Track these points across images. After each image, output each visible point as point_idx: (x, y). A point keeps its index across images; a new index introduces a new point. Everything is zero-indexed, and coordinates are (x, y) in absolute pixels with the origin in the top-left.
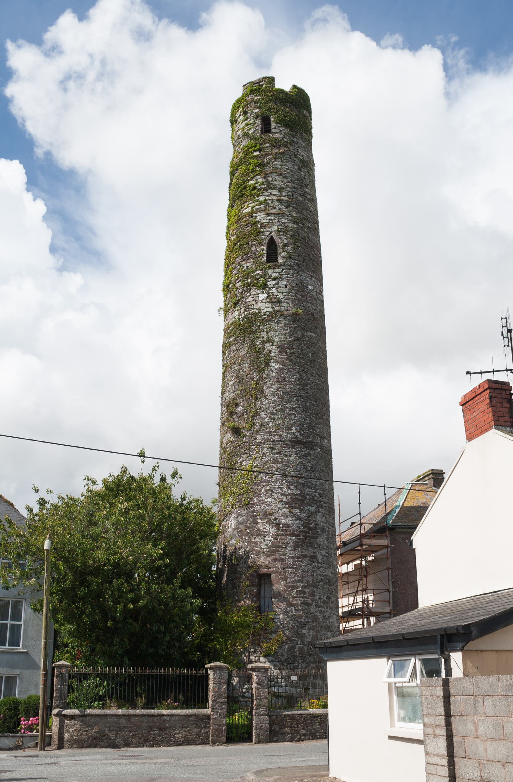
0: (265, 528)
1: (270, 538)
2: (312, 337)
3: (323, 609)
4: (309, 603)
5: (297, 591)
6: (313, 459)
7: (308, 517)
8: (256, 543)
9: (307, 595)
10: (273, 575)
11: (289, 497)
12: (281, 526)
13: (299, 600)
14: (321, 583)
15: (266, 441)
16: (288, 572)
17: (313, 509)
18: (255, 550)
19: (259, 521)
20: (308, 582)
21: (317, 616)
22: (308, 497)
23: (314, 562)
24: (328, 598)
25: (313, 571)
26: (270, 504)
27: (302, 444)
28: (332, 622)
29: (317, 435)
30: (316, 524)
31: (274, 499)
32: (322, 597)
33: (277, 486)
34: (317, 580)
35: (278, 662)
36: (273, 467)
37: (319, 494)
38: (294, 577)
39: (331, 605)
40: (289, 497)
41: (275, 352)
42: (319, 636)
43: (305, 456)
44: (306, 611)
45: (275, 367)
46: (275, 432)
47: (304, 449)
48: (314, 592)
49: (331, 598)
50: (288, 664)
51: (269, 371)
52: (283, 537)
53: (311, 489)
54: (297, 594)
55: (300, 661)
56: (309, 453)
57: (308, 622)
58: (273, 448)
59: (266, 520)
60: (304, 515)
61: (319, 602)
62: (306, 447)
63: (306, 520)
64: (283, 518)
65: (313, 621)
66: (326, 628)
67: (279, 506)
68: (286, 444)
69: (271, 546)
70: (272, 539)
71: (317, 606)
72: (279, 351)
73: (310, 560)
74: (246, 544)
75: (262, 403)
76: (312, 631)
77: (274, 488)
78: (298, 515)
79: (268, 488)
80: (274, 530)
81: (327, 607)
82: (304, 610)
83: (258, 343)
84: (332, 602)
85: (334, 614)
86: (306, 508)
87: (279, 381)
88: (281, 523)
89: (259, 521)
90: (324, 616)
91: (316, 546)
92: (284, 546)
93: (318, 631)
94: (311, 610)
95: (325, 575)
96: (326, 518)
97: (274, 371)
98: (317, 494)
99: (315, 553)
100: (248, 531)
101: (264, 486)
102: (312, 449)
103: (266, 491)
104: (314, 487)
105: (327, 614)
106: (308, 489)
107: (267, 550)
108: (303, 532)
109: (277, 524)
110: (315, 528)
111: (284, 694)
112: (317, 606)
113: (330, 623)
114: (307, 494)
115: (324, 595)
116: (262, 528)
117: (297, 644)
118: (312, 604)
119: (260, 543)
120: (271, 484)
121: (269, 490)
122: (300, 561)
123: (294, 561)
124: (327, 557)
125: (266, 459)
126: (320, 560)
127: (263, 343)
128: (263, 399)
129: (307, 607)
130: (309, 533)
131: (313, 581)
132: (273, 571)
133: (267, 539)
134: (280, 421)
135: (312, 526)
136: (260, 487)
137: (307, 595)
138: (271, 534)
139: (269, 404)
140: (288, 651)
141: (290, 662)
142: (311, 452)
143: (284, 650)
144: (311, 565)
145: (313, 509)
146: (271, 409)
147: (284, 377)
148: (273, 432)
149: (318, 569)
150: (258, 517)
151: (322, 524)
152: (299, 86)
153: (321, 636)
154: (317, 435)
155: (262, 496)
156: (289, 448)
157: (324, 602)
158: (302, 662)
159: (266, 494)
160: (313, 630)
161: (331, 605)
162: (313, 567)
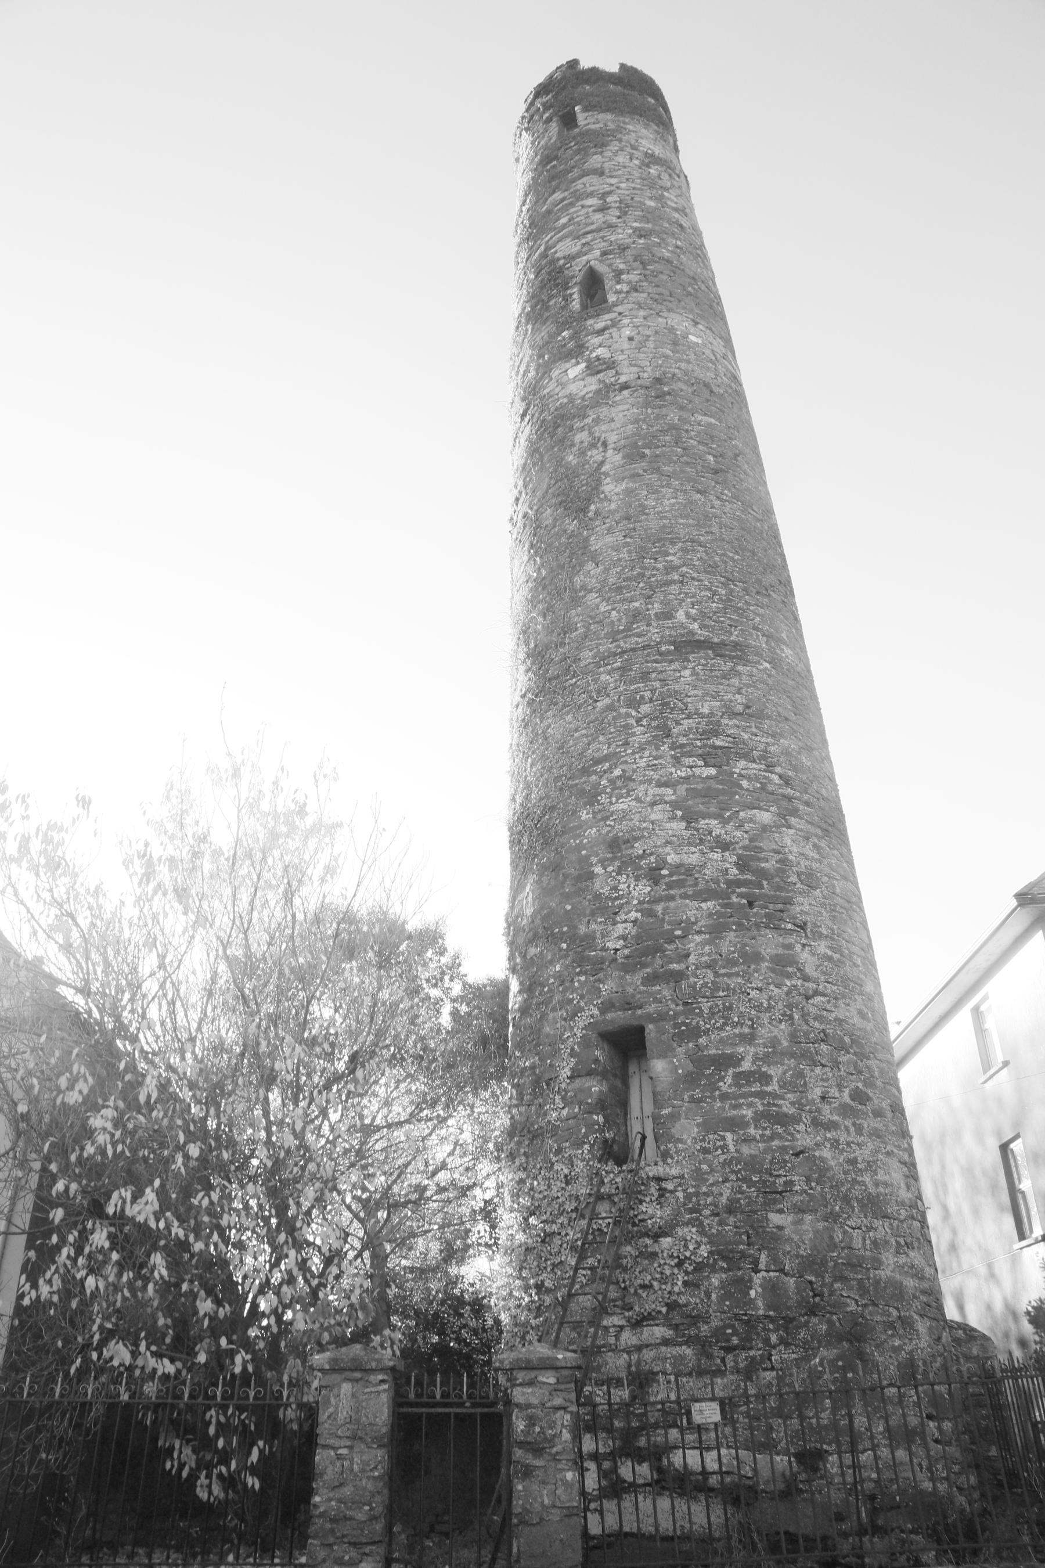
0: (615, 888)
1: (634, 915)
2: (710, 424)
3: (843, 1137)
4: (786, 1115)
5: (737, 1076)
6: (748, 686)
7: (751, 840)
8: (591, 937)
9: (774, 1087)
10: (650, 1027)
11: (682, 790)
12: (665, 872)
13: (750, 1105)
14: (824, 1047)
15: (603, 659)
16: (701, 1015)
17: (765, 817)
18: (589, 958)
19: (598, 870)
20: (774, 1042)
21: (822, 1159)
22: (745, 783)
23: (789, 976)
24: (858, 1096)
25: (790, 1006)
26: (625, 815)
27: (711, 648)
28: (886, 1184)
29: (755, 628)
30: (784, 861)
31: (638, 799)
32: (834, 1092)
33: (642, 763)
34: (806, 1034)
35: (686, 1343)
36: (628, 715)
37: (781, 777)
38: (721, 1029)
39: (870, 1123)
40: (682, 790)
41: (614, 458)
42: (839, 1236)
43: (724, 677)
44: (776, 1143)
45: (617, 490)
46: (628, 629)
47: (719, 661)
48: (801, 1075)
49: (869, 1099)
50: (729, 1350)
51: (602, 501)
52: (672, 904)
53: (754, 761)
54: (740, 1086)
55: (774, 1338)
56: (732, 669)
57: (791, 1183)
58: (623, 669)
59: (617, 863)
60: (738, 834)
61: (826, 1109)
62: (722, 656)
63: (744, 848)
64: (668, 849)
65: (808, 1180)
66: (863, 1206)
67: (653, 817)
68: (661, 654)
69: (638, 938)
70: (639, 915)
71: (816, 1123)
72: (624, 457)
73: (773, 970)
74: (564, 946)
75: (588, 574)
76: (808, 1218)
77: (634, 771)
78: (718, 837)
79: (618, 772)
80: (642, 889)
81: (859, 1130)
82: (772, 1138)
83: (571, 458)
84: (878, 1114)
85: (888, 1154)
86: (742, 814)
87: (628, 518)
88: (665, 862)
89: (598, 870)
90: (853, 1162)
91: (789, 926)
92: (678, 933)
93: (833, 1217)
94: (794, 1139)
95: (836, 1019)
96: (815, 846)
97: (615, 498)
98: (775, 778)
99: (789, 947)
100: (568, 907)
101: (605, 772)
102: (744, 660)
103: (612, 782)
104: (763, 758)
105: (863, 1154)
106: (742, 763)
107: (626, 951)
108: (739, 883)
109: (652, 869)
110: (781, 872)
111: (713, 1481)
112: (816, 1123)
113: (877, 1184)
114: (740, 775)
115: (840, 1087)
116: (606, 891)
117: (756, 1271)
118: (797, 1120)
119: (603, 936)
120: (626, 762)
121: (619, 777)
122: (737, 974)
123: (716, 974)
124: (839, 964)
125: (608, 701)
126: (810, 970)
127: (582, 453)
128: (590, 566)
129: (780, 1129)
130: (761, 887)
131: (794, 1038)
132: (650, 1018)
133: (624, 917)
134: (637, 604)
135: (770, 865)
136: (594, 777)
137: (774, 1087)
138: (635, 902)
139: (607, 570)
140: (722, 1299)
141: (735, 1341)
142: (740, 668)
143: (708, 1294)
144: (778, 986)
145: (765, 817)
146: (612, 580)
147: (641, 505)
148: (623, 631)
149: (808, 998)
150: (594, 860)
151: (803, 863)
152: (629, 63)
153: (845, 1232)
154: (755, 628)
155: (603, 799)
156: (671, 661)
157: (845, 1110)
158: (782, 1341)
159: (613, 789)
160: (813, 1211)
161: (870, 1123)
162: (788, 993)
